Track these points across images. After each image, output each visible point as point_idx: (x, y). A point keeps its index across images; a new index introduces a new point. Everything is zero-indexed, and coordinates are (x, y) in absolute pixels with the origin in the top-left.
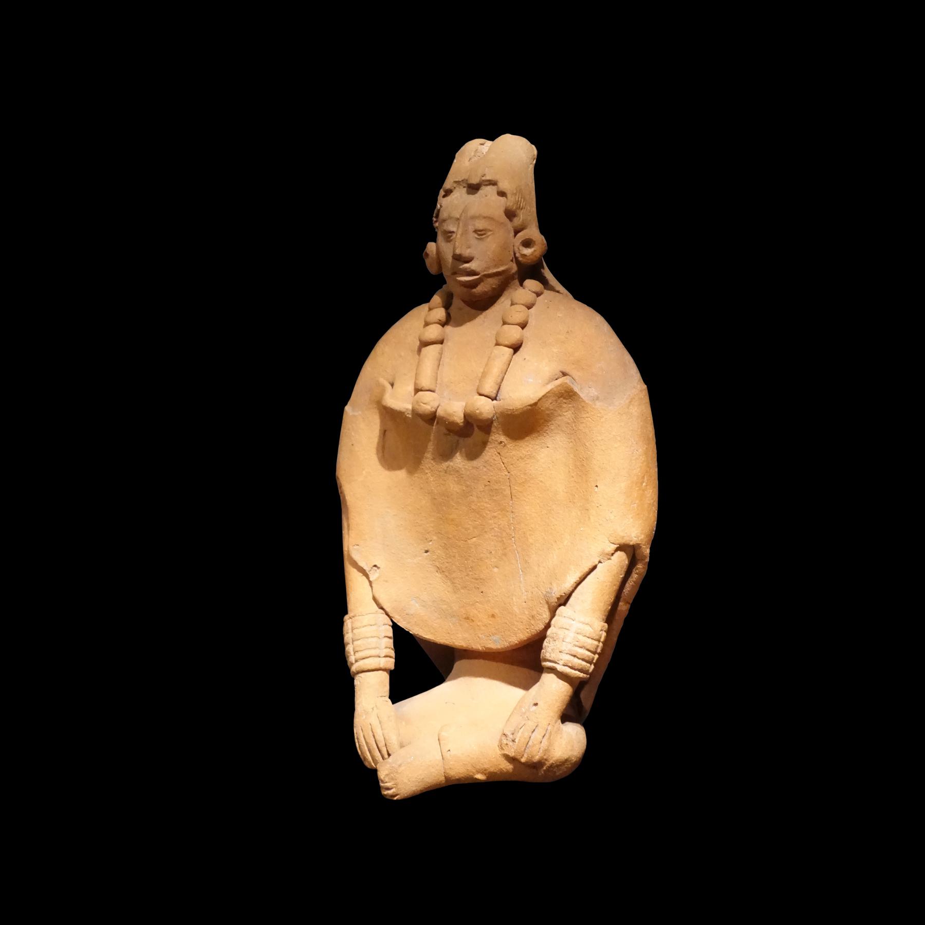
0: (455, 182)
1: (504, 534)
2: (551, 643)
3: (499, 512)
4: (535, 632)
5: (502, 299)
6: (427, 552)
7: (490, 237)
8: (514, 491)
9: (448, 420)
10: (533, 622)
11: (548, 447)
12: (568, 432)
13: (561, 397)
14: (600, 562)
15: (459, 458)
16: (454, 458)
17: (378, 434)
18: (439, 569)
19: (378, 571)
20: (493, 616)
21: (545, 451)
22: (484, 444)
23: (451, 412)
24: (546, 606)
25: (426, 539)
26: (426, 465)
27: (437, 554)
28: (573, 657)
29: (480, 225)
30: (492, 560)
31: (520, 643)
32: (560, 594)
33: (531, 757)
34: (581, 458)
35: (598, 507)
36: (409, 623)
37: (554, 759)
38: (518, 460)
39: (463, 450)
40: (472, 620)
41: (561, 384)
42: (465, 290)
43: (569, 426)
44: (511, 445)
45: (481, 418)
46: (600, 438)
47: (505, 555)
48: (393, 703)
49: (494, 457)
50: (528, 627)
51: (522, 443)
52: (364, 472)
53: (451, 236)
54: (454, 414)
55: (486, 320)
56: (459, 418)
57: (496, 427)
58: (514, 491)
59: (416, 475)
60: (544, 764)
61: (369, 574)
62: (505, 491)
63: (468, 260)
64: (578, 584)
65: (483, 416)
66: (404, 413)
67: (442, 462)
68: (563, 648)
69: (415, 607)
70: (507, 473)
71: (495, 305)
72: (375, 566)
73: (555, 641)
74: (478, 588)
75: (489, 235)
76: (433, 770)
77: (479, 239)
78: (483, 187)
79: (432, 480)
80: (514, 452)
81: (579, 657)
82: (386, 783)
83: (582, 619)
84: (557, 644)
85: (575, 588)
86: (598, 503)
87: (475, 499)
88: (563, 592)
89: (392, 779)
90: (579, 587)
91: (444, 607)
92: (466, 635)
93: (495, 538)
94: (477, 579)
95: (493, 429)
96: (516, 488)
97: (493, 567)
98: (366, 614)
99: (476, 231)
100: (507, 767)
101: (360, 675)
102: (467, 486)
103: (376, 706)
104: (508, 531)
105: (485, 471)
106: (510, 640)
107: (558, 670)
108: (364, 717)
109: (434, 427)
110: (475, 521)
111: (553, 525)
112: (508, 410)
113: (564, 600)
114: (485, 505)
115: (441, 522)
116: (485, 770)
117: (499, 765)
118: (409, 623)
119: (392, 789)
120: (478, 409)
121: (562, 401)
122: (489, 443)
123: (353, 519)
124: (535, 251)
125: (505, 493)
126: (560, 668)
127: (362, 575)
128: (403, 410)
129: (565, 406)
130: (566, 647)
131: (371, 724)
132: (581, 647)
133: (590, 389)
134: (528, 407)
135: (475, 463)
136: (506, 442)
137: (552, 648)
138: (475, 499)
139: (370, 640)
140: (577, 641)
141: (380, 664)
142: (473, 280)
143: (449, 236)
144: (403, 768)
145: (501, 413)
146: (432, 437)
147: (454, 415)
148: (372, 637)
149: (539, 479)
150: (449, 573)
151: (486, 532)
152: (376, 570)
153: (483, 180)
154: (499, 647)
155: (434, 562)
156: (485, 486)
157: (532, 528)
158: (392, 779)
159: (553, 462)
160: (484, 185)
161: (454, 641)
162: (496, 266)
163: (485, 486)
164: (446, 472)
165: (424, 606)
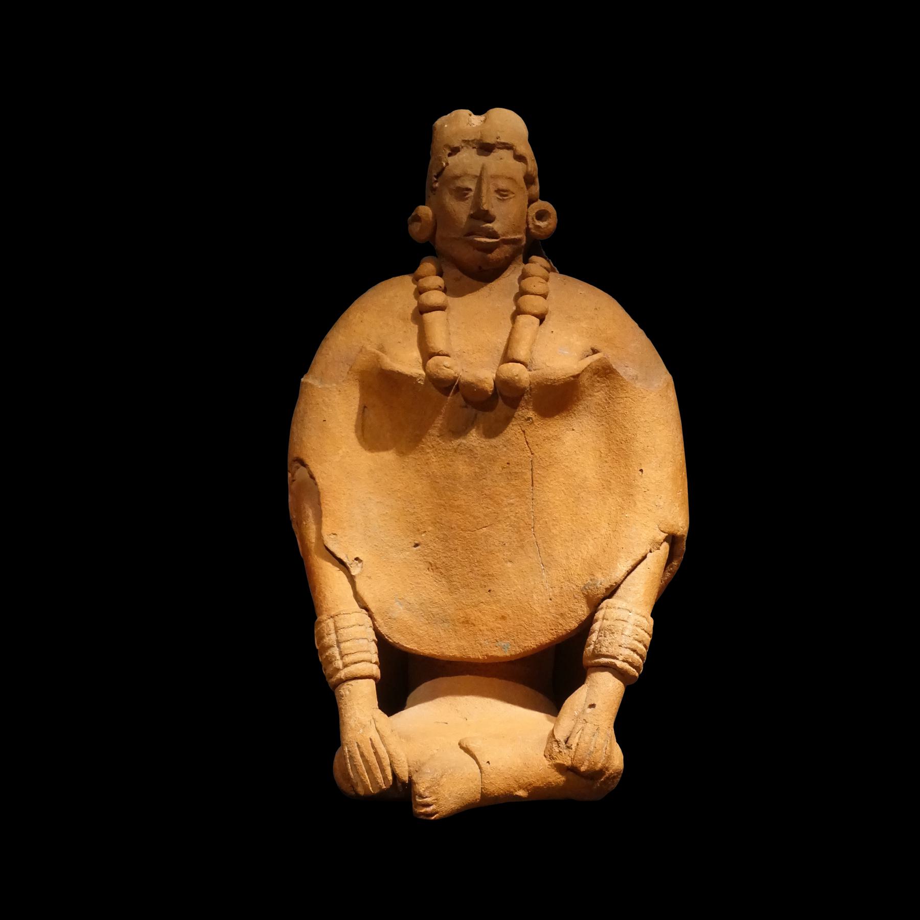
0: (464, 141)
1: (522, 524)
2: (608, 636)
3: (518, 499)
4: (564, 633)
5: (507, 273)
6: (416, 545)
7: (512, 200)
8: (535, 476)
9: (477, 386)
10: (561, 621)
11: (573, 430)
12: (599, 415)
13: (596, 374)
14: (651, 552)
15: (474, 435)
16: (468, 434)
17: (357, 411)
18: (432, 566)
19: (360, 565)
20: (503, 618)
21: (570, 433)
22: (508, 420)
23: (483, 378)
24: (584, 601)
25: (418, 530)
26: (428, 443)
27: (432, 547)
28: (632, 652)
29: (503, 184)
30: (505, 554)
31: (539, 647)
32: (610, 584)
33: (594, 765)
34: (617, 441)
35: (645, 492)
36: (390, 628)
37: (614, 768)
38: (544, 440)
39: (481, 426)
40: (472, 624)
41: (600, 359)
42: (479, 254)
43: (599, 407)
44: (538, 421)
45: (518, 385)
46: (642, 419)
47: (522, 547)
48: (389, 716)
49: (518, 435)
50: (553, 628)
51: (550, 422)
52: (340, 452)
53: (467, 194)
54: (486, 380)
55: (492, 292)
56: (489, 386)
57: (526, 400)
58: (536, 476)
59: (410, 456)
60: (604, 774)
61: (350, 567)
62: (526, 474)
63: (491, 219)
64: (629, 573)
65: (521, 384)
66: (415, 378)
67: (452, 439)
68: (623, 642)
69: (399, 611)
70: (530, 454)
71: (501, 277)
72: (357, 559)
73: (613, 633)
74: (485, 586)
75: (511, 198)
76: (471, 785)
77: (500, 199)
78: (496, 150)
79: (434, 460)
80: (540, 432)
81: (639, 652)
82: (427, 797)
83: (639, 611)
84: (615, 636)
85: (624, 579)
86: (644, 488)
87: (489, 482)
88: (614, 581)
89: (434, 793)
90: (628, 577)
91: (435, 610)
92: (463, 643)
93: (511, 528)
94: (484, 576)
95: (522, 403)
96: (538, 472)
97: (506, 562)
98: (353, 613)
99: (498, 191)
100: (558, 778)
101: (350, 683)
102: (482, 468)
103: (373, 718)
104: (527, 520)
105: (505, 451)
106: (526, 645)
107: (618, 665)
108: (361, 731)
109: (449, 398)
110: (487, 508)
111: (584, 514)
112: (547, 380)
113: (612, 592)
114: (501, 489)
115: (442, 509)
116: (530, 785)
117: (548, 777)
118: (390, 628)
119: (432, 805)
120: (517, 376)
121: (596, 378)
122: (513, 419)
123: (327, 504)
124: (549, 224)
125: (526, 477)
126: (619, 664)
127: (338, 569)
128: (415, 375)
129: (597, 384)
130: (624, 640)
131: (371, 739)
132: (640, 642)
133: (627, 368)
134: (571, 378)
135: (494, 441)
136: (534, 418)
137: (610, 641)
138: (489, 482)
139: (361, 641)
140: (637, 635)
141: (372, 671)
142: (492, 243)
143: (464, 193)
144: (444, 780)
145: (538, 383)
146: (443, 411)
147: (485, 381)
148: (363, 639)
149: (564, 464)
150: (447, 570)
151: (499, 521)
152: (357, 564)
153: (498, 142)
154: (508, 654)
155: (425, 558)
156: (503, 468)
157: (556, 517)
158: (434, 793)
159: (579, 446)
160: (499, 148)
161: (444, 650)
162: (515, 232)
163: (503, 468)
164: (455, 452)
165: (409, 610)
